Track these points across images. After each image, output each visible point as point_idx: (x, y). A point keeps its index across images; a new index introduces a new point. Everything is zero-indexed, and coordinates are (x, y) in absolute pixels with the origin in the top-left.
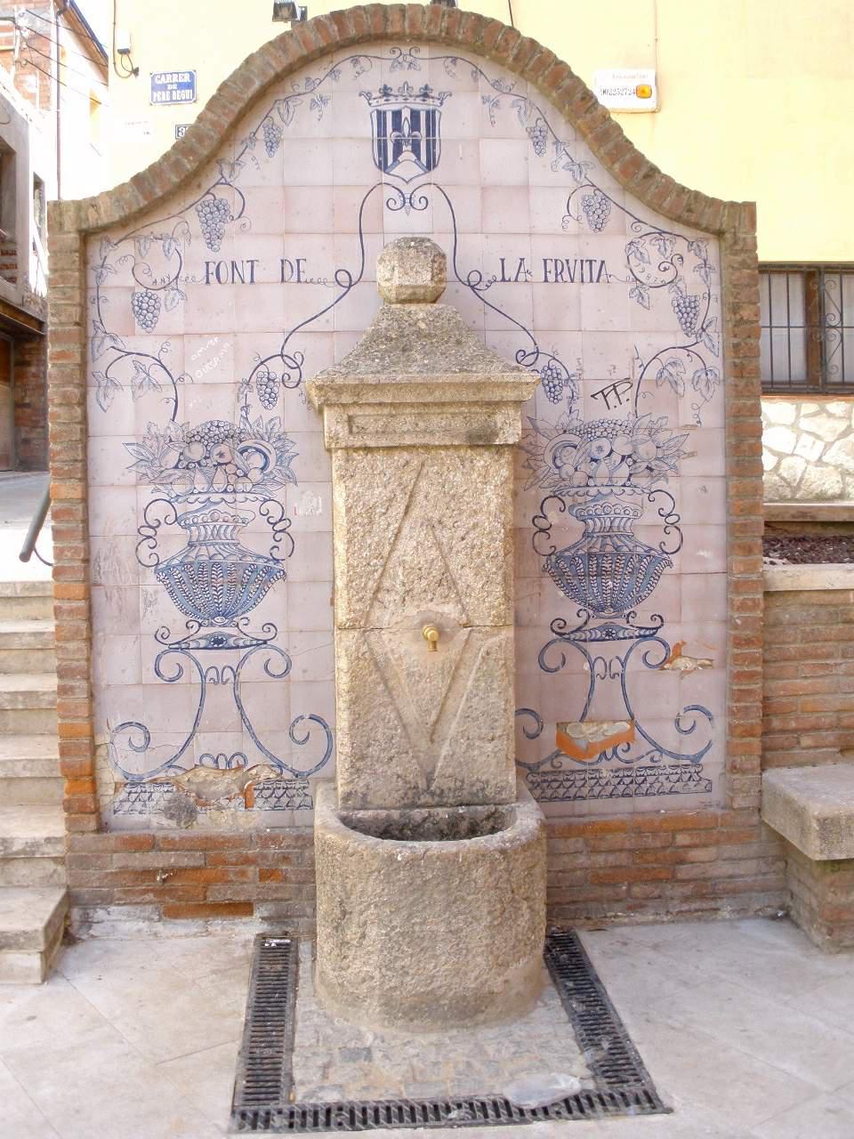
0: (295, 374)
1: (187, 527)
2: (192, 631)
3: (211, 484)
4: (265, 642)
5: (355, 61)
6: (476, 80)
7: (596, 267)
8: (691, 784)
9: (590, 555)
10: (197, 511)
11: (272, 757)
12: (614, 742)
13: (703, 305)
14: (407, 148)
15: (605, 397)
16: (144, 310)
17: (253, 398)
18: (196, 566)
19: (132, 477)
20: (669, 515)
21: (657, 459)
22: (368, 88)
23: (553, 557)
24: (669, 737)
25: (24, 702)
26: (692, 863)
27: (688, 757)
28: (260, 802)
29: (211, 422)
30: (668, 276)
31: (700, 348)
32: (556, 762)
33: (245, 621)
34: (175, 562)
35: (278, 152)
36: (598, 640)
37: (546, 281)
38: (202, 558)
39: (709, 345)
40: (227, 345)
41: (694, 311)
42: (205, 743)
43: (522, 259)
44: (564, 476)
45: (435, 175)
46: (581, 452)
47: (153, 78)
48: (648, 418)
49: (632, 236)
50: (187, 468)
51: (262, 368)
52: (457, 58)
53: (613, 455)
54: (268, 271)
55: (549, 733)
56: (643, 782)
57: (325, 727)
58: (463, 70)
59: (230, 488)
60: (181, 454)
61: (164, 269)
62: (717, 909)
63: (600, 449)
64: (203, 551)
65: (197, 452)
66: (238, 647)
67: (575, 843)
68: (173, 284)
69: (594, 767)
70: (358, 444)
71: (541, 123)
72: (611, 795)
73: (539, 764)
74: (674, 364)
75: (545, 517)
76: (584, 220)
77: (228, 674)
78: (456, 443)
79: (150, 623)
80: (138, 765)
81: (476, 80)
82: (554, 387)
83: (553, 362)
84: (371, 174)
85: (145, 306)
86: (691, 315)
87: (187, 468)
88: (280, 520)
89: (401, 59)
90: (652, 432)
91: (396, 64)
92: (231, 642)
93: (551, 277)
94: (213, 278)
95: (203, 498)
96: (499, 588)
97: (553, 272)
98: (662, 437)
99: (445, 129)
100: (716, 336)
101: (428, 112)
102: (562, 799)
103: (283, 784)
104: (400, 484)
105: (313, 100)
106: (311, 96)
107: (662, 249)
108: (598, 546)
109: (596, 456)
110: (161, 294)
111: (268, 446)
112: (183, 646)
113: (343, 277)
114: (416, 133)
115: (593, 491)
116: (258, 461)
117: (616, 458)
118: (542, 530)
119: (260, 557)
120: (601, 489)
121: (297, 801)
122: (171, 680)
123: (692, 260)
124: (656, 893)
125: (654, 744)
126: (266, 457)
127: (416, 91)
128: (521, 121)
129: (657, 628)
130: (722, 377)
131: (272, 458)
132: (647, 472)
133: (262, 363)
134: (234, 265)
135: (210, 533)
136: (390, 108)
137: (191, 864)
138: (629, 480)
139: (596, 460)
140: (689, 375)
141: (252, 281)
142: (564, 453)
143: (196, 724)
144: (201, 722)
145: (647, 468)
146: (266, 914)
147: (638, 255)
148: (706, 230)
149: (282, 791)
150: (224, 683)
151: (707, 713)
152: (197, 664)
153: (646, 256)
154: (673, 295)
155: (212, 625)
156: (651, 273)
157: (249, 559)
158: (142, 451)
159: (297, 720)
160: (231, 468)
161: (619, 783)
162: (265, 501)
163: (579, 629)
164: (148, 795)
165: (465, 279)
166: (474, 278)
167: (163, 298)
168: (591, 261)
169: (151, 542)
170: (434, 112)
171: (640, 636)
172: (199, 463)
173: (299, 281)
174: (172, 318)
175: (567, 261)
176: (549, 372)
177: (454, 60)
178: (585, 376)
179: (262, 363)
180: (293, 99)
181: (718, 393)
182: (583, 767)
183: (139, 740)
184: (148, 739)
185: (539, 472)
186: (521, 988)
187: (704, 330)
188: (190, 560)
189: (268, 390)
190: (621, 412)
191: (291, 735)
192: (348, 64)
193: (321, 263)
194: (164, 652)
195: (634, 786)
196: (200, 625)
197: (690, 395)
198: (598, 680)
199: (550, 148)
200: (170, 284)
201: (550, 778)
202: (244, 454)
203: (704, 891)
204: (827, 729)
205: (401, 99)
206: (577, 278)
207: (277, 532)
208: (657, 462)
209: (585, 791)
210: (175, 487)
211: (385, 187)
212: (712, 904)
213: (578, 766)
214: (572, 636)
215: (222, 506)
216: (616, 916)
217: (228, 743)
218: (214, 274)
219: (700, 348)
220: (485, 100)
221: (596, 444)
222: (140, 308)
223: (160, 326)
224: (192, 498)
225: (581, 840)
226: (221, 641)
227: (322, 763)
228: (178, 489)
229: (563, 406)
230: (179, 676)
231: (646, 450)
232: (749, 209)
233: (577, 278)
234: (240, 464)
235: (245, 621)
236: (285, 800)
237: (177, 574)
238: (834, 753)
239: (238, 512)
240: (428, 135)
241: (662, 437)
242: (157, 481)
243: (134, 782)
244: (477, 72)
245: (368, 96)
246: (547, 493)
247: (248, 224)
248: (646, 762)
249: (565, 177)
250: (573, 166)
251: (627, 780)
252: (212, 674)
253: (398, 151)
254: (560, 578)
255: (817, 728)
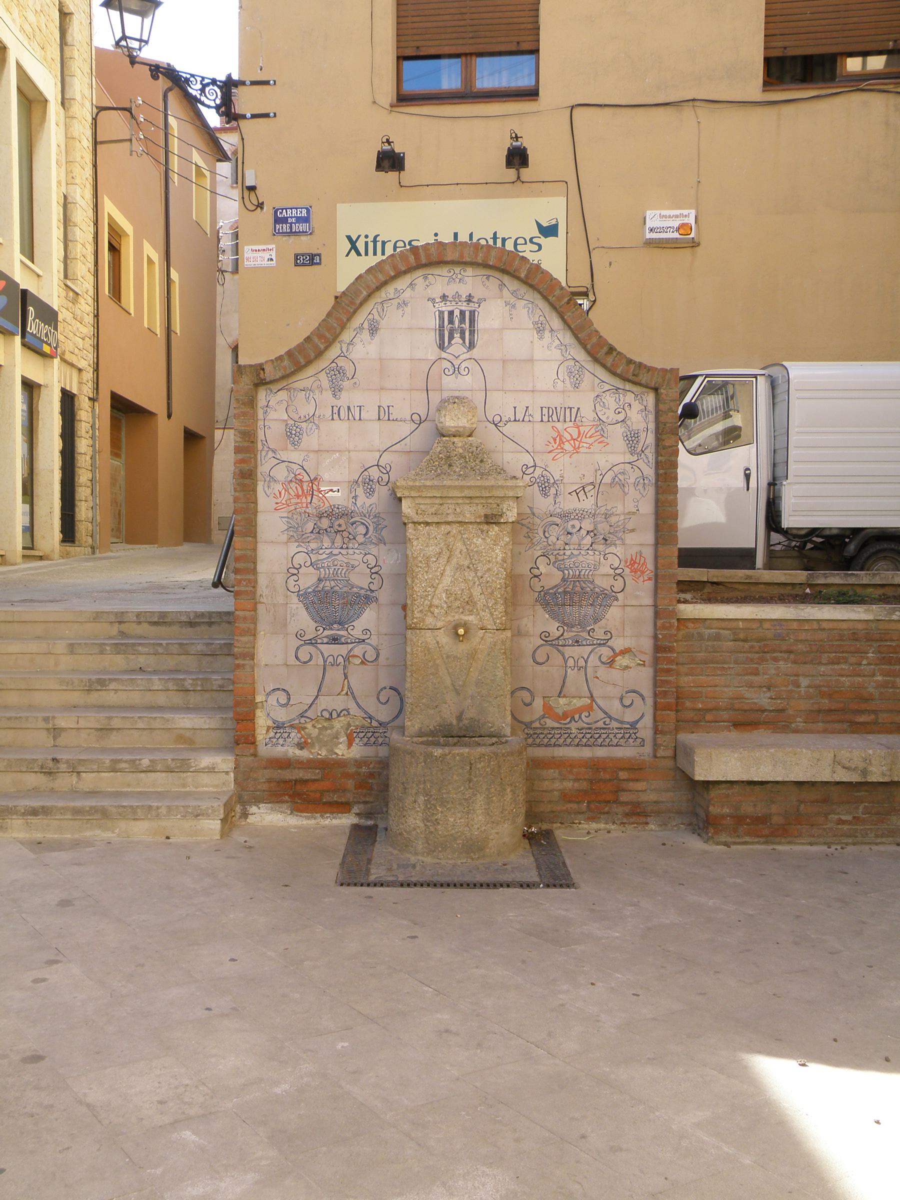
0: (385, 477)
1: (318, 569)
2: (319, 633)
3: (333, 543)
4: (364, 640)
5: (425, 277)
6: (501, 290)
7: (574, 411)
8: (631, 740)
9: (565, 592)
10: (324, 559)
11: (366, 712)
12: (580, 710)
13: (643, 436)
14: (457, 336)
15: (577, 494)
16: (293, 435)
17: (360, 491)
18: (322, 593)
19: (284, 538)
20: (616, 569)
21: (610, 533)
22: (434, 296)
23: (542, 593)
24: (615, 707)
25: (202, 685)
26: (630, 791)
27: (628, 723)
28: (357, 740)
29: (334, 505)
30: (621, 417)
31: (640, 463)
32: (542, 722)
33: (352, 627)
34: (310, 590)
35: (377, 338)
36: (569, 646)
37: (542, 421)
38: (326, 588)
39: (646, 461)
40: (344, 458)
41: (637, 439)
42: (325, 702)
43: (527, 407)
44: (550, 543)
45: (475, 353)
46: (561, 528)
47: (276, 212)
48: (605, 507)
49: (598, 391)
50: (319, 533)
51: (366, 473)
52: (490, 276)
53: (582, 531)
54: (370, 413)
55: (538, 703)
56: (599, 738)
57: (399, 694)
58: (493, 283)
59: (345, 546)
60: (315, 524)
61: (307, 410)
62: (647, 823)
63: (573, 526)
64: (328, 584)
65: (325, 523)
66: (347, 643)
67: (552, 773)
68: (311, 419)
69: (567, 726)
70: (421, 520)
71: (542, 318)
72: (578, 745)
73: (532, 722)
74: (624, 473)
75: (538, 568)
76: (567, 382)
77: (340, 660)
78: (478, 521)
79: (293, 628)
80: (282, 716)
81: (501, 290)
82: (545, 487)
83: (545, 472)
84: (433, 352)
85: (294, 432)
86: (635, 442)
87: (319, 533)
88: (375, 566)
89: (454, 277)
90: (607, 516)
91: (451, 280)
92: (343, 640)
93: (545, 418)
94: (336, 416)
95: (328, 551)
96: (503, 607)
97: (547, 415)
98: (613, 520)
99: (480, 324)
100: (650, 454)
101: (470, 312)
102: (546, 746)
103: (372, 730)
104: (445, 544)
105: (399, 303)
106: (397, 300)
107: (617, 400)
108: (571, 587)
109: (570, 530)
110: (304, 425)
111: (369, 521)
112: (313, 642)
113: (416, 417)
114: (463, 325)
115: (568, 553)
116: (362, 529)
117: (583, 532)
118: (535, 576)
119: (362, 588)
120: (573, 551)
121: (380, 740)
122: (305, 663)
123: (637, 406)
124: (607, 809)
125: (606, 713)
126: (367, 527)
127: (464, 298)
128: (529, 317)
129: (608, 640)
130: (654, 482)
131: (371, 529)
132: (603, 541)
133: (365, 470)
134: (349, 408)
135: (331, 572)
136: (446, 308)
137: (313, 778)
138: (591, 546)
139: (570, 534)
140: (632, 480)
141: (360, 419)
142: (551, 528)
143: (319, 690)
144: (323, 689)
145: (603, 538)
146: (358, 811)
147: (602, 404)
148: (646, 387)
149: (371, 734)
150: (338, 665)
151: (641, 696)
152: (322, 653)
153: (607, 404)
154: (623, 429)
155: (331, 629)
156: (609, 415)
157: (355, 589)
158: (291, 522)
159: (381, 690)
160: (345, 534)
161: (583, 737)
162: (366, 554)
163: (558, 638)
164: (287, 734)
165: (491, 420)
166: (497, 419)
167: (305, 428)
168: (571, 408)
169: (295, 578)
170: (474, 311)
171: (597, 644)
172: (326, 530)
173: (389, 420)
174: (310, 441)
175: (556, 408)
176: (542, 479)
177: (488, 277)
178: (565, 481)
179: (365, 470)
180: (386, 302)
181: (651, 492)
182: (560, 726)
183: (283, 700)
184: (289, 699)
185: (535, 540)
186: (507, 840)
187: (643, 452)
188: (319, 589)
189: (369, 487)
190: (588, 504)
191: (378, 699)
192: (421, 279)
193: (402, 410)
194: (301, 645)
195: (592, 740)
196: (324, 629)
197: (632, 493)
198: (569, 670)
199: (547, 334)
200: (309, 420)
201: (538, 731)
202: (354, 525)
203: (638, 811)
204: (724, 710)
205: (454, 303)
206: (562, 419)
207: (373, 573)
208: (610, 535)
209: (561, 741)
210: (310, 544)
211: (443, 360)
212: (643, 820)
213: (556, 725)
214: (554, 643)
215: (340, 557)
216: (580, 823)
217: (338, 703)
218: (336, 413)
219: (640, 463)
220: (507, 304)
221: (571, 523)
222: (291, 433)
223: (304, 444)
224: (321, 551)
225: (557, 771)
226: (337, 639)
227: (397, 717)
228: (313, 545)
229: (550, 499)
230: (310, 660)
231: (603, 528)
232: (678, 369)
233: (562, 419)
234: (351, 532)
235: (352, 627)
236: (373, 739)
237: (311, 597)
238: (729, 726)
239: (349, 561)
240: (470, 326)
241: (613, 520)
242: (300, 540)
243: (278, 726)
244: (502, 285)
245: (433, 300)
246: (540, 553)
247: (358, 383)
248: (600, 724)
249: (556, 354)
250: (563, 346)
251: (588, 736)
252: (331, 659)
253: (451, 337)
254: (546, 605)
255: (717, 709)
